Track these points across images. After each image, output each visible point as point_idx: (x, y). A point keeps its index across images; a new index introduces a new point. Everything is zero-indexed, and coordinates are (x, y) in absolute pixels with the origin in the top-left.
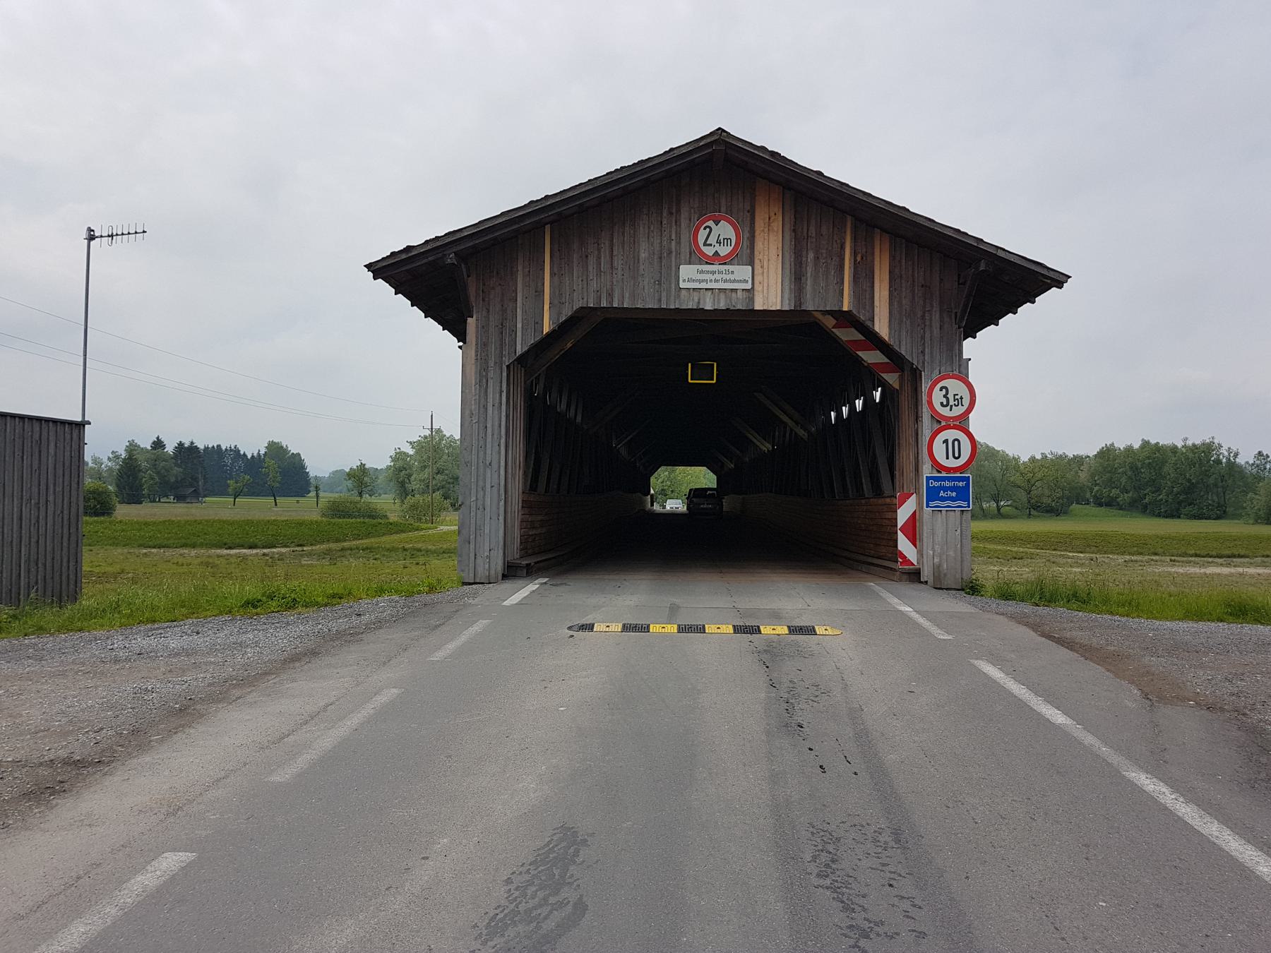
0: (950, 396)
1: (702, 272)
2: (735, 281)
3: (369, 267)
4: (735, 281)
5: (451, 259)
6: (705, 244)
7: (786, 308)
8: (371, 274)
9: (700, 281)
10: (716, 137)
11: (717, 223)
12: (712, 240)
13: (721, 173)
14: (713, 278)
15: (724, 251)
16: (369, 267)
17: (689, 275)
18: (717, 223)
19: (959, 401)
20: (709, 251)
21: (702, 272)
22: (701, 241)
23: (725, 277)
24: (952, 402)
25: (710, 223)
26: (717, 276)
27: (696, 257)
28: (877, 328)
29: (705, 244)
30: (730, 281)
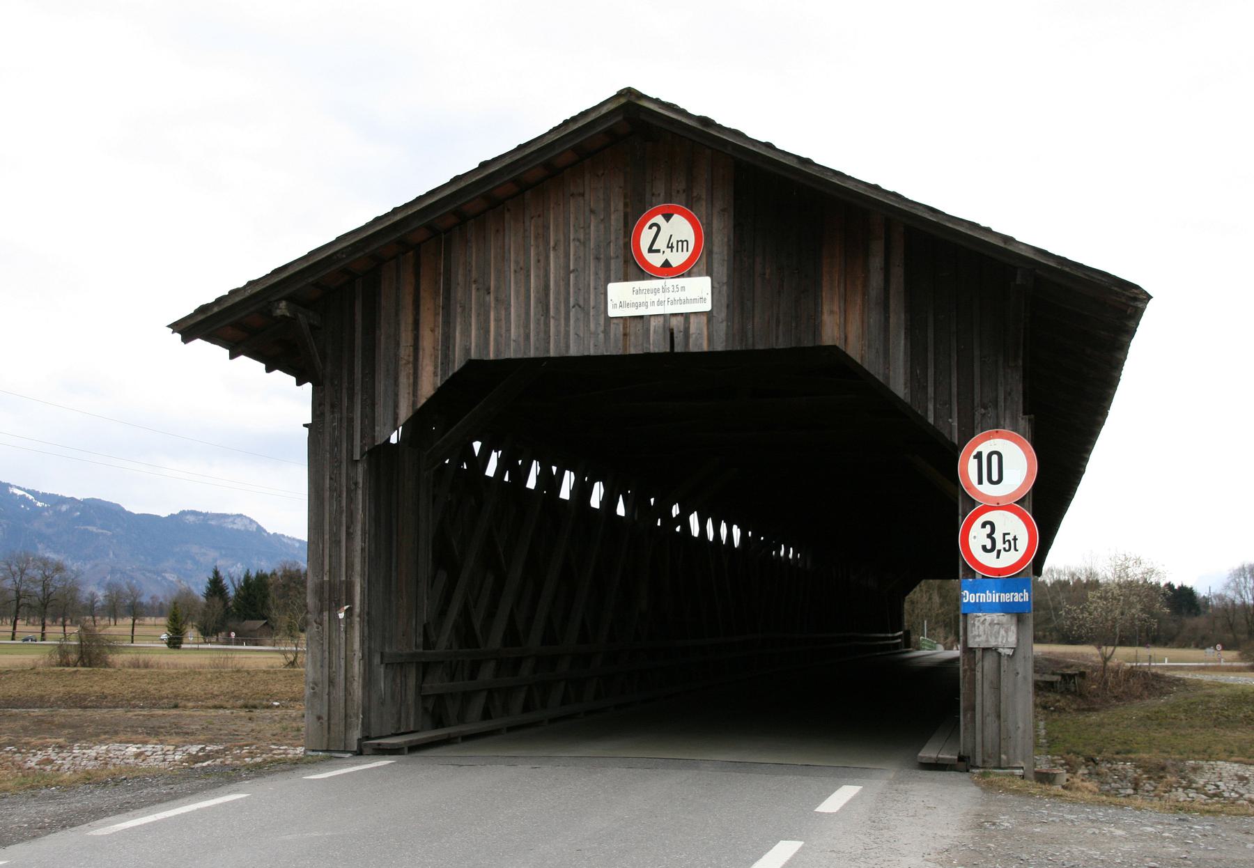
0: (998, 536)
1: (638, 292)
2: (686, 301)
3: (175, 327)
4: (686, 301)
5: (282, 309)
6: (651, 250)
7: (720, 347)
8: (178, 336)
9: (637, 305)
10: (623, 101)
11: (668, 217)
12: (661, 244)
13: (633, 151)
14: (655, 298)
15: (677, 259)
16: (175, 327)
17: (625, 299)
18: (668, 217)
19: (1011, 544)
20: (656, 260)
21: (638, 292)
22: (645, 243)
23: (672, 296)
24: (999, 545)
25: (659, 219)
26: (661, 296)
27: (636, 269)
28: (892, 388)
29: (651, 250)
30: (681, 301)
